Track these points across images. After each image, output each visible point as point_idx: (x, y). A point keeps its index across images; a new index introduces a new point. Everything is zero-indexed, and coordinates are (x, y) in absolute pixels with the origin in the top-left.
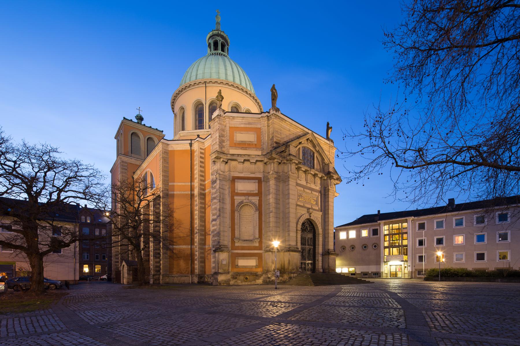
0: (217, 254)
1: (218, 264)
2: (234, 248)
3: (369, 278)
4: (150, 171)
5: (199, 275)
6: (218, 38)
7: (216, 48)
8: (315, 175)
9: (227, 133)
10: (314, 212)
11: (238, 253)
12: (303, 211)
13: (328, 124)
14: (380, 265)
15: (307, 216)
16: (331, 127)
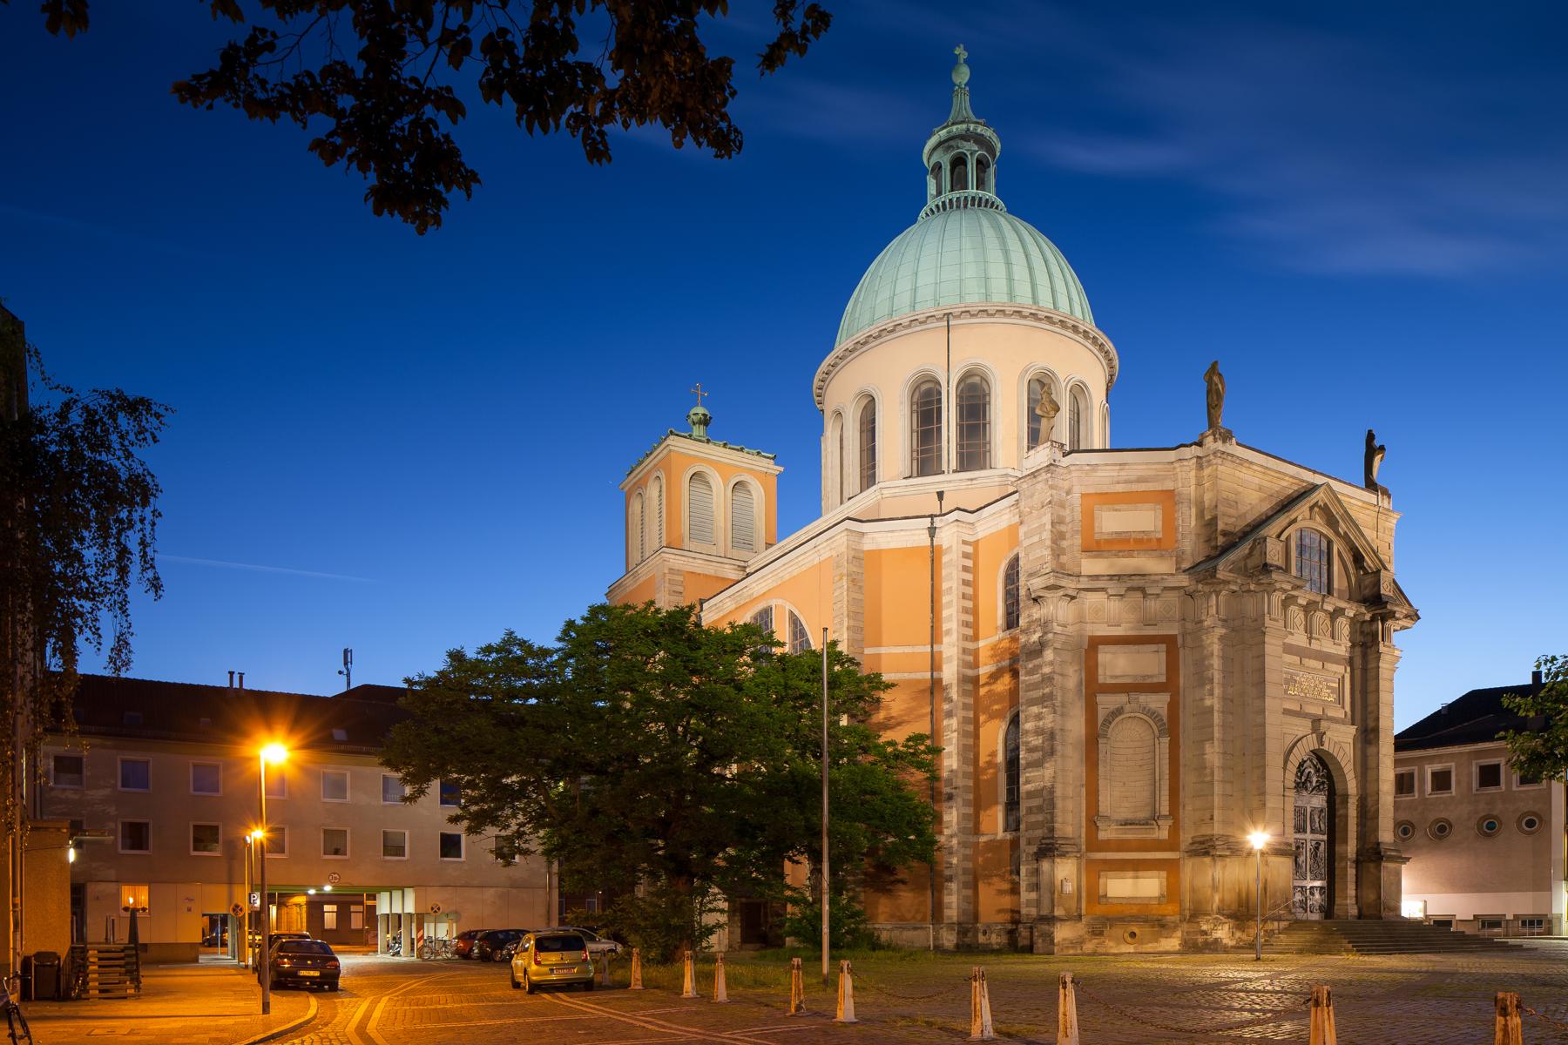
0: (1045, 865)
1: (1053, 893)
2: (1094, 844)
3: (1507, 936)
4: (788, 607)
5: (959, 924)
6: (968, 147)
7: (959, 182)
8: (1338, 612)
9: (1074, 512)
10: (1334, 726)
11: (1105, 861)
12: (1302, 727)
13: (1371, 437)
14: (1550, 889)
15: (1311, 743)
16: (1382, 448)
